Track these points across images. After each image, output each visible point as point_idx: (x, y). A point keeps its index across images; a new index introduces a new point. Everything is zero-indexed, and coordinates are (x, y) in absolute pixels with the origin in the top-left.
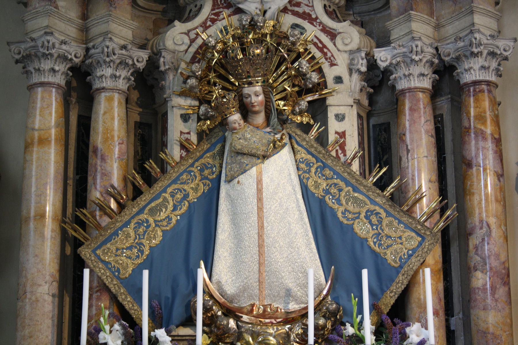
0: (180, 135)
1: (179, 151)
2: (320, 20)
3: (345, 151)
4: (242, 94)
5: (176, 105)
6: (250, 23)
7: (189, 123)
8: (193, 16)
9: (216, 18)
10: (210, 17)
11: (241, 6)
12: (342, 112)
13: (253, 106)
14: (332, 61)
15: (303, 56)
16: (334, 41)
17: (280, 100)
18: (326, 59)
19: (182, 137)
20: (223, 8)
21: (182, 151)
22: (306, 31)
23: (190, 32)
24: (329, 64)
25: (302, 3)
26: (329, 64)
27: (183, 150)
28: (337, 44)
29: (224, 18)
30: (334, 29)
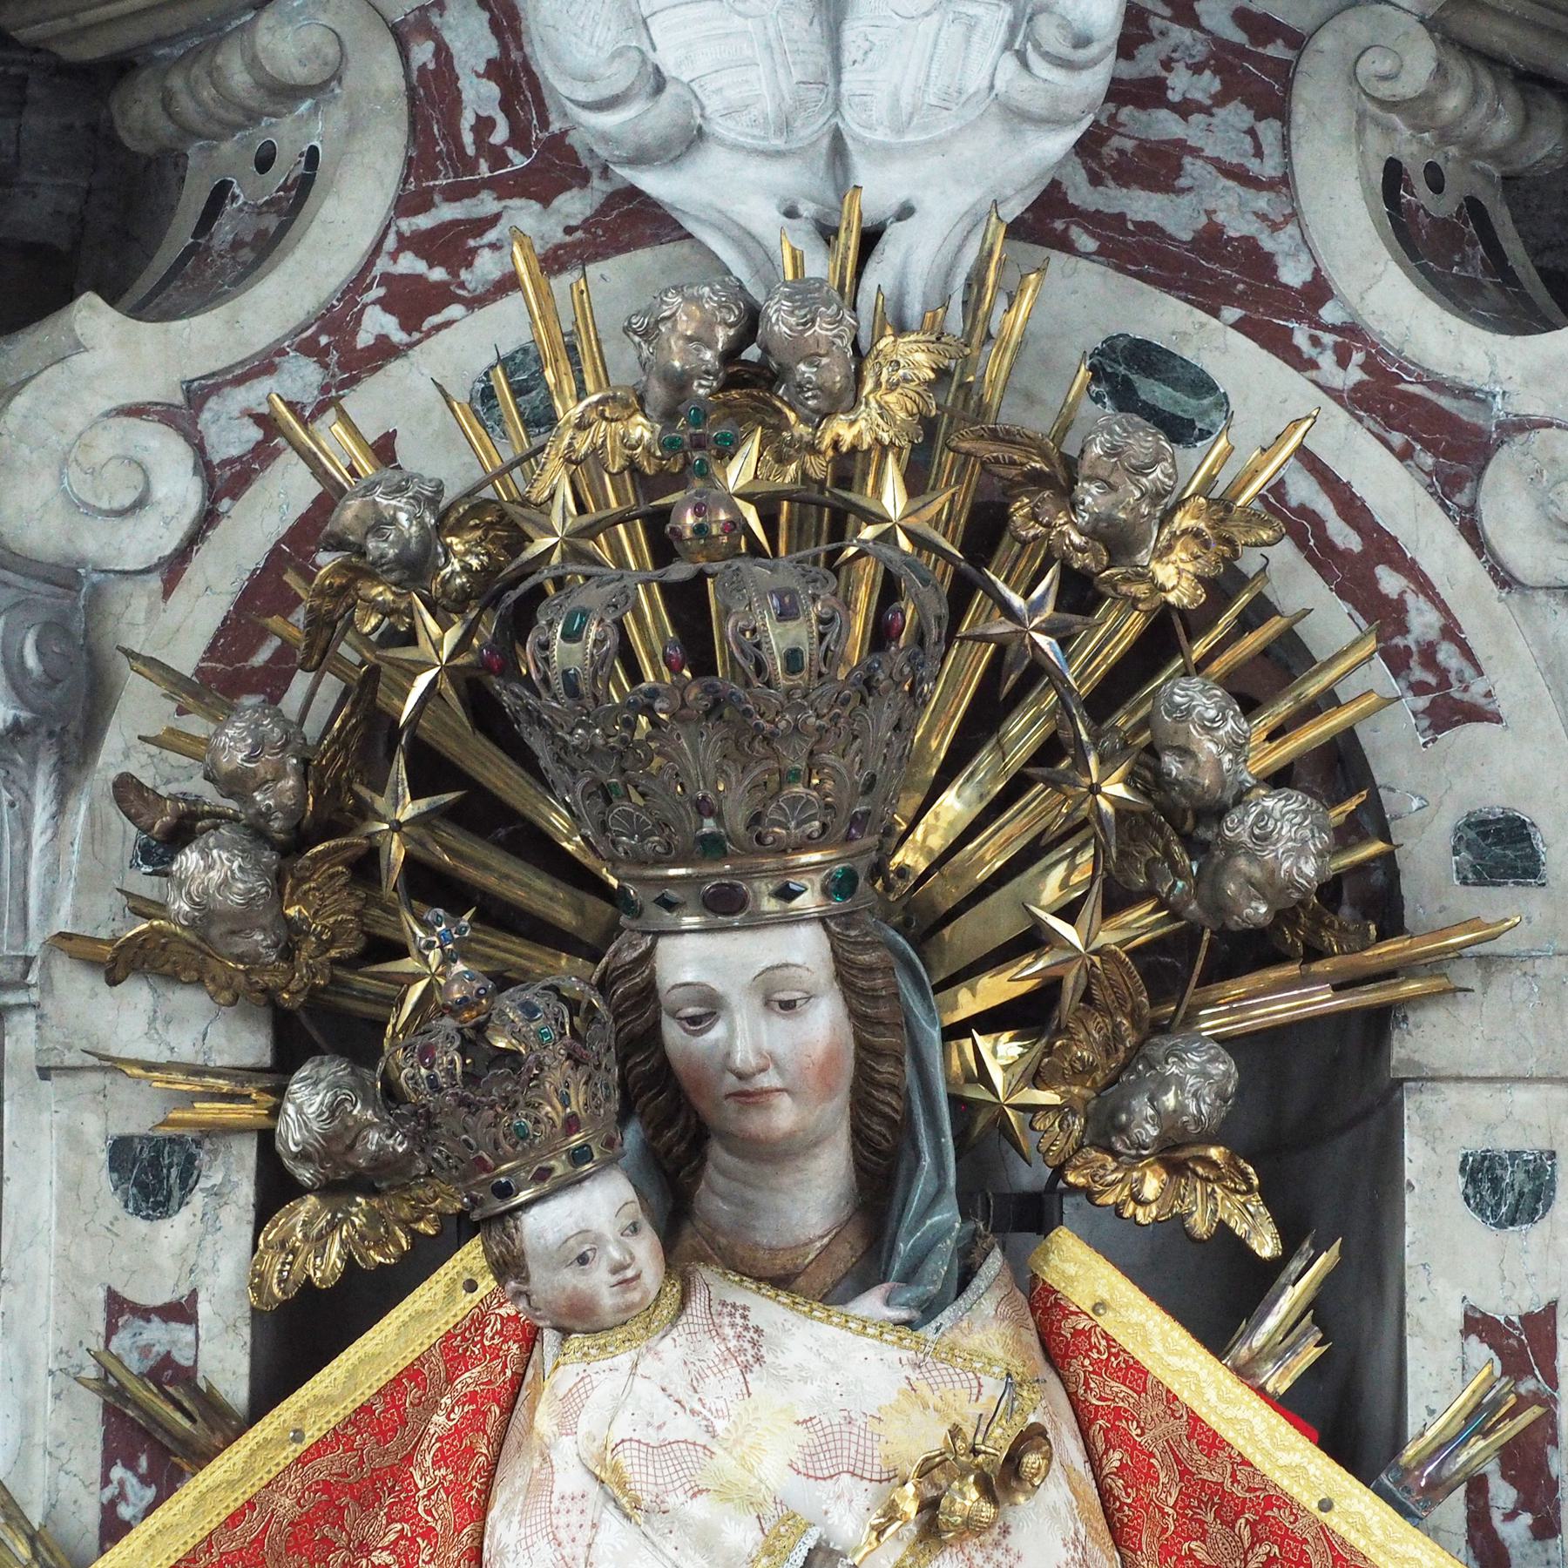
0: (101, 1328)
1: (96, 1473)
2: (1345, 304)
3: (1553, 1486)
4: (648, 992)
5: (71, 1059)
6: (730, 356)
7: (183, 1217)
8: (237, 245)
9: (438, 274)
10: (382, 265)
11: (652, 182)
12: (1529, 1143)
13: (751, 1098)
14: (1444, 683)
15: (1192, 637)
16: (1463, 499)
17: (991, 1021)
18: (1397, 661)
19: (120, 1342)
20: (506, 188)
21: (118, 1472)
22: (1223, 402)
23: (212, 403)
24: (1423, 702)
25: (1196, 152)
26: (1423, 702)
27: (130, 1465)
28: (1490, 526)
29: (509, 283)
30: (1467, 393)
